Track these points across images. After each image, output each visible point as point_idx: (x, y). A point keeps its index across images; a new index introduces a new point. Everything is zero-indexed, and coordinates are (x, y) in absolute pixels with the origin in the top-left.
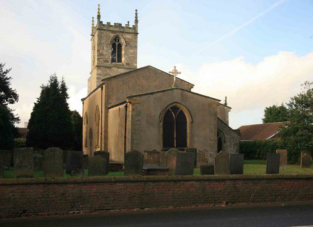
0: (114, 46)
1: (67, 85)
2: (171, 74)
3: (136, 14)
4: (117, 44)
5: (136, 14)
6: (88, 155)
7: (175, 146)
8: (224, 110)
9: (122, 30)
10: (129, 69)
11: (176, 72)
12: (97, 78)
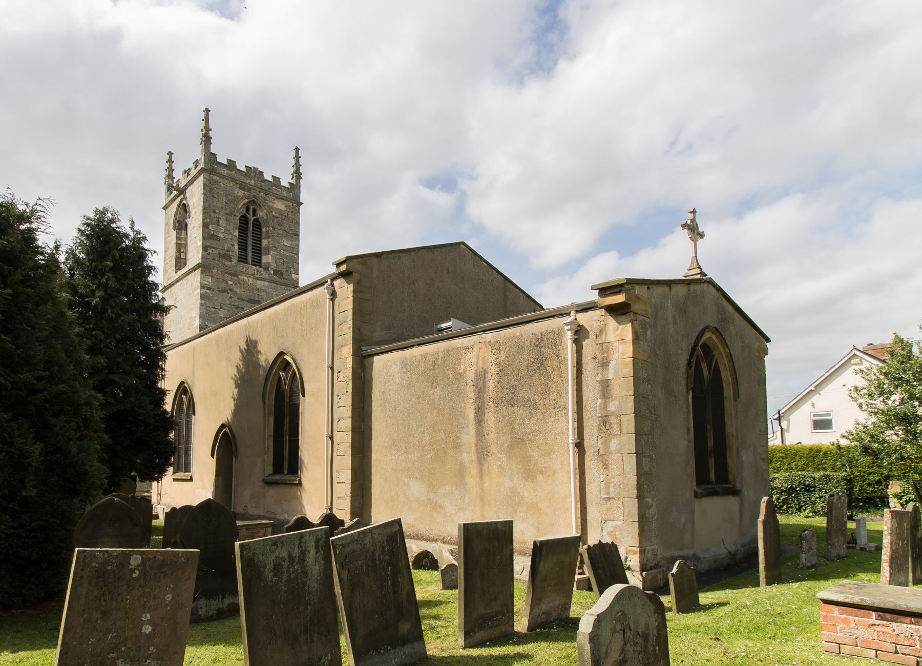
0: (244, 220)
1: (342, 257)
3: (297, 157)
4: (251, 219)
5: (297, 157)
6: (141, 481)
7: (712, 476)
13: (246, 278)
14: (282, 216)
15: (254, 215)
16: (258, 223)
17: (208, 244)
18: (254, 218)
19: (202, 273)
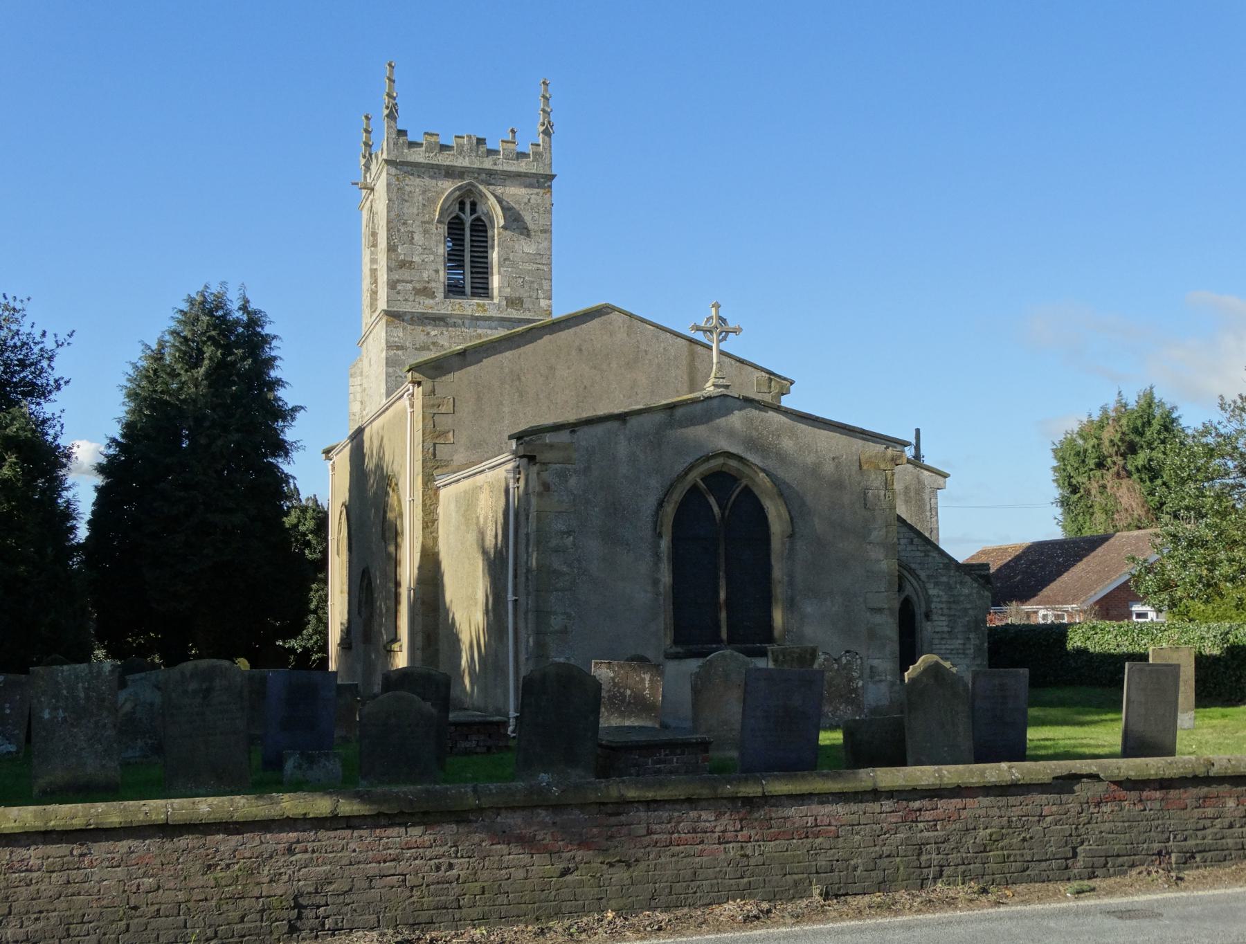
0: (455, 228)
2: (699, 336)
4: (468, 219)
7: (724, 635)
8: (920, 482)
9: (488, 164)
10: (520, 321)
11: (723, 328)
12: (390, 362)
13: (460, 321)
14: (520, 204)
15: (473, 211)
16: (480, 223)
17: (397, 277)
18: (474, 217)
19: (387, 325)
